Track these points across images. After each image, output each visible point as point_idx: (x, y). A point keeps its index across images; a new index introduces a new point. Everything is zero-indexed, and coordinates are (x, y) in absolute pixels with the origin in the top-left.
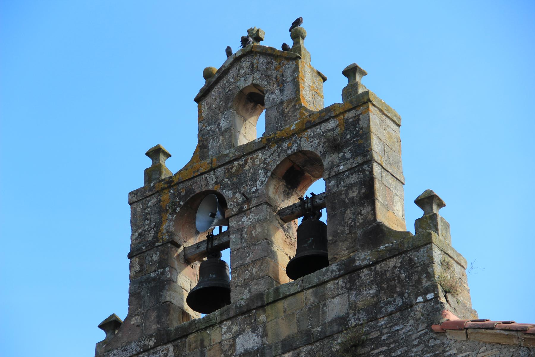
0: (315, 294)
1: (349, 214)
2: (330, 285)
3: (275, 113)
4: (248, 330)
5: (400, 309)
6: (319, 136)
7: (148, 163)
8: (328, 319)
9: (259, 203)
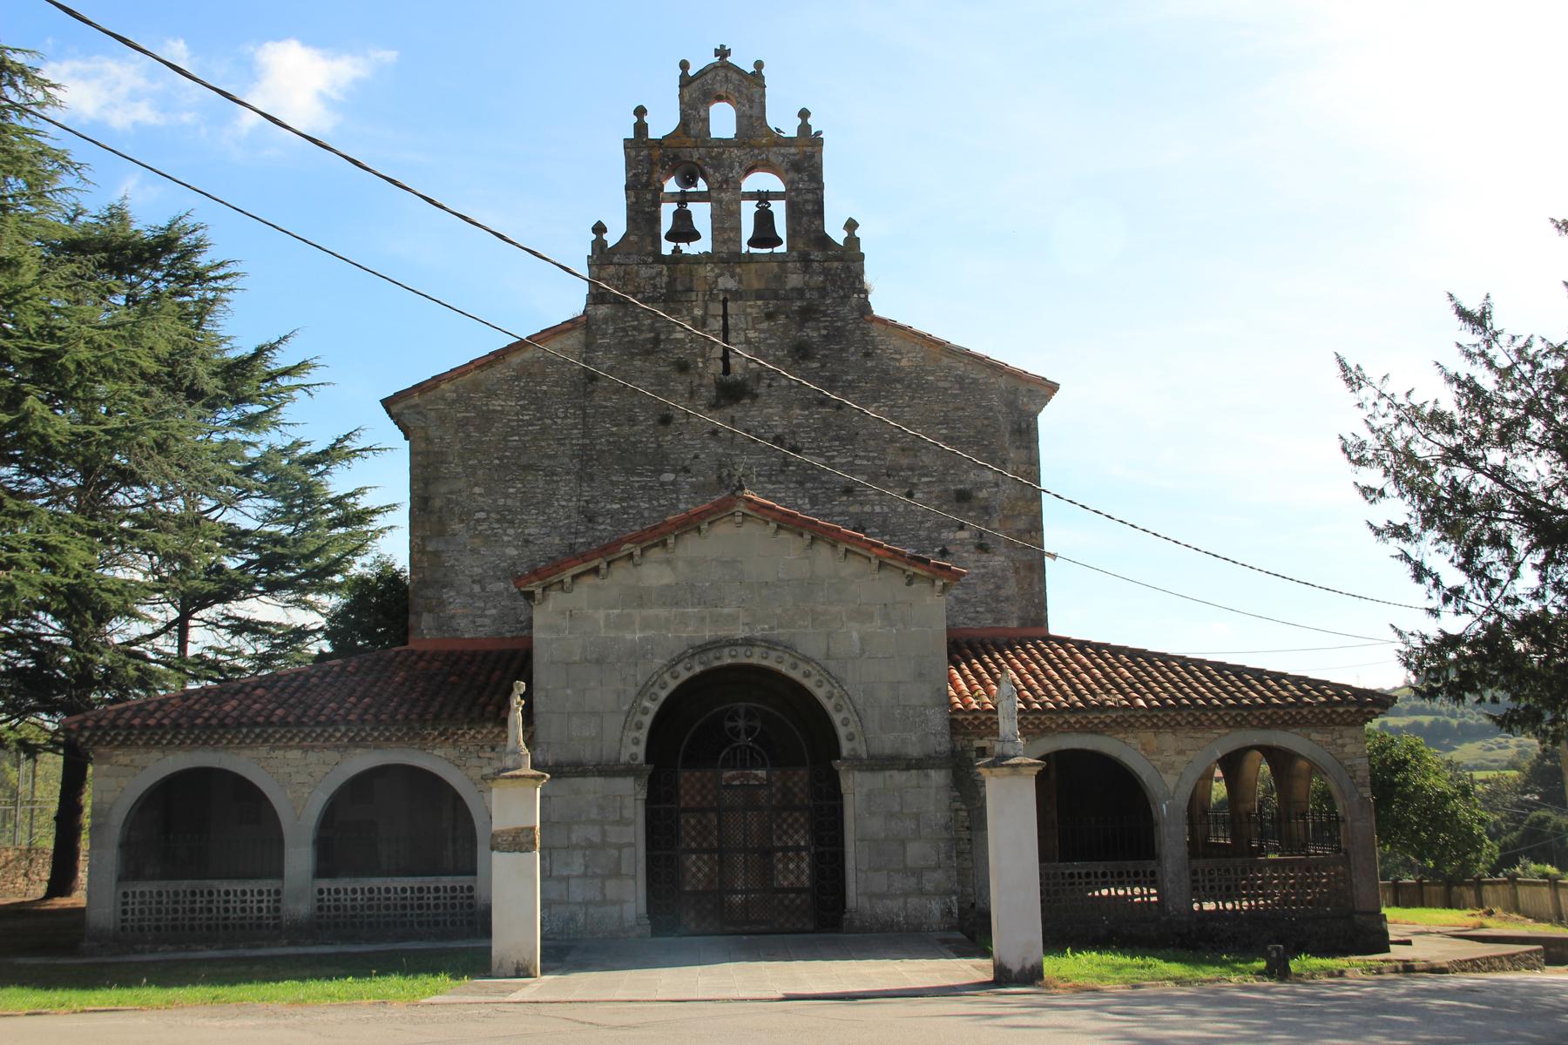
0: (779, 266)
1: (805, 219)
2: (789, 264)
3: (746, 123)
4: (727, 274)
5: (842, 297)
6: (784, 156)
7: (635, 119)
8: (517, 414)
9: (990, 1022)
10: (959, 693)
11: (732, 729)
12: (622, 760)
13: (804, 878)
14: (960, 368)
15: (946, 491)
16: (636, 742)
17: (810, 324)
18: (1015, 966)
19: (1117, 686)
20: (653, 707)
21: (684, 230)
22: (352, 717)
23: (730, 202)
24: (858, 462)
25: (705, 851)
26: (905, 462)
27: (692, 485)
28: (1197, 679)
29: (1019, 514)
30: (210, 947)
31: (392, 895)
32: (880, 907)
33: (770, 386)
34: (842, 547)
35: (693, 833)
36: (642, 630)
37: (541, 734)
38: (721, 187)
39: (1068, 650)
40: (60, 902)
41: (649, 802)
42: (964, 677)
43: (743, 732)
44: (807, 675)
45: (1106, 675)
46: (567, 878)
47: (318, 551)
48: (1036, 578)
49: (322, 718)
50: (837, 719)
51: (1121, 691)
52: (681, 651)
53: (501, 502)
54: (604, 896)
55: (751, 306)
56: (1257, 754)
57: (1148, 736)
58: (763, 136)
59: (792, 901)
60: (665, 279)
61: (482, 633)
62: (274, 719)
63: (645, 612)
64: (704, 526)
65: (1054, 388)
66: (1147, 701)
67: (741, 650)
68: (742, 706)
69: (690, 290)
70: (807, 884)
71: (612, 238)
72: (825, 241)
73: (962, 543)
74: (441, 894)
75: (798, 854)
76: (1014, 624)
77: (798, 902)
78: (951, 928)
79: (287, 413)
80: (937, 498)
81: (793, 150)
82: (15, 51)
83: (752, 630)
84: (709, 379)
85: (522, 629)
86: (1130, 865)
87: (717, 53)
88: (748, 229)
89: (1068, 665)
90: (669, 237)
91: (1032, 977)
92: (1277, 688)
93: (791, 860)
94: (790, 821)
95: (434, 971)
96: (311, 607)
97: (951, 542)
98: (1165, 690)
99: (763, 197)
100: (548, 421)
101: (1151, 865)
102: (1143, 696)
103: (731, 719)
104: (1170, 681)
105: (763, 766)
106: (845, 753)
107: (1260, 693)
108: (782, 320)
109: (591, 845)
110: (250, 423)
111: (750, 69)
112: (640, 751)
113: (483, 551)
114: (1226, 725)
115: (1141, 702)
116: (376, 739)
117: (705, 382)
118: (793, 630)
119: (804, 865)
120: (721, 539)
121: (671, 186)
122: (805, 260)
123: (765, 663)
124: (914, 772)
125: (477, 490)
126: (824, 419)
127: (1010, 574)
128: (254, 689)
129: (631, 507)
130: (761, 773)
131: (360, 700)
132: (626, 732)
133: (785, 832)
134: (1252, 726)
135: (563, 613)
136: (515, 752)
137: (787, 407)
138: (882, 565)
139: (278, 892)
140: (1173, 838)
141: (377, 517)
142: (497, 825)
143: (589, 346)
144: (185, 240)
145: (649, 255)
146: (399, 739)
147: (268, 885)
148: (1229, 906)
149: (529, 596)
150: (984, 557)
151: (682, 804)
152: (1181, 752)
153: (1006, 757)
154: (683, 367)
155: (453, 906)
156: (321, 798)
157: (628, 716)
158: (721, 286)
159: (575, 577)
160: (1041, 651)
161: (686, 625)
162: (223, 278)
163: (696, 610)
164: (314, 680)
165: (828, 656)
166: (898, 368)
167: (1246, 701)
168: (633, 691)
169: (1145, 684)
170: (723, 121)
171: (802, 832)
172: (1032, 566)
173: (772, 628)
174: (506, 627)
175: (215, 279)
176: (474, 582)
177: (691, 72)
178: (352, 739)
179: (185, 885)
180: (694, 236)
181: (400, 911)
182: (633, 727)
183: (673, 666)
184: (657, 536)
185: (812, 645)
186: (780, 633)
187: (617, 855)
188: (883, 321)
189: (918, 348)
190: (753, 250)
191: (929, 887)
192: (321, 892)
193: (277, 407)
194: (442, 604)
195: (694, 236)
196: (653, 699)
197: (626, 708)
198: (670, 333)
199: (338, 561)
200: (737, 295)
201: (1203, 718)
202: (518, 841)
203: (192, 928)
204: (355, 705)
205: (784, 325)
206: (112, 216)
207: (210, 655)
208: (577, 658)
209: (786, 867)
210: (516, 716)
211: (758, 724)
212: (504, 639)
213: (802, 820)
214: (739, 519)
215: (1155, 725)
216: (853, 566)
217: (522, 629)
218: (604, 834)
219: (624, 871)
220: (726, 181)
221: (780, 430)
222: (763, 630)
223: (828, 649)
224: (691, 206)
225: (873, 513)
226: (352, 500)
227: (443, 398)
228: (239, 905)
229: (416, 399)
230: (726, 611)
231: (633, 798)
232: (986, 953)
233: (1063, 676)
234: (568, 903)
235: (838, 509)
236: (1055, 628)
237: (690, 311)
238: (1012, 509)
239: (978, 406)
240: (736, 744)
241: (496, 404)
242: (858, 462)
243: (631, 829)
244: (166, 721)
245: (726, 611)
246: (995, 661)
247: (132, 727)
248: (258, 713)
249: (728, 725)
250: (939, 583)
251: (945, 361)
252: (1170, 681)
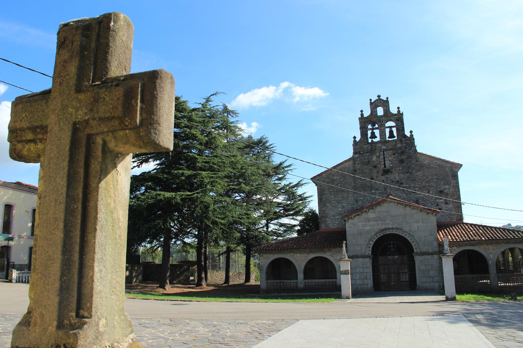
1: (400, 132)
5: (410, 148)
7: (361, 113)
10: (441, 238)
11: (390, 247)
12: (366, 254)
13: (407, 279)
14: (439, 163)
15: (437, 191)
16: (369, 251)
17: (403, 155)
18: (450, 297)
19: (478, 235)
20: (372, 243)
21: (373, 136)
22: (309, 247)
23: (383, 129)
24: (416, 185)
26: (427, 185)
27: (379, 193)
28: (498, 233)
29: (455, 195)
30: (284, 293)
31: (320, 283)
32: (424, 285)
33: (395, 170)
34: (412, 207)
35: (382, 270)
36: (369, 227)
37: (349, 249)
38: (381, 126)
39: (468, 226)
40: (248, 284)
41: (372, 263)
42: (442, 234)
44: (406, 235)
45: (476, 232)
46: (356, 279)
47: (297, 207)
48: (460, 209)
49: (304, 247)
50: (413, 244)
51: (479, 236)
53: (337, 199)
54: (364, 283)
55: (390, 152)
56: (518, 249)
57: (486, 246)
58: (389, 114)
60: (370, 148)
61: (335, 227)
62: (294, 248)
64: (381, 204)
65: (461, 165)
66: (485, 238)
67: (391, 230)
68: (391, 242)
69: (376, 150)
70: (408, 280)
71: (358, 139)
72: (405, 136)
73: (442, 202)
74: (330, 283)
76: (455, 220)
78: (441, 290)
79: (288, 176)
80: (435, 192)
81: (396, 117)
84: (381, 169)
85: (344, 226)
86: (483, 275)
87: (378, 96)
88: (388, 135)
89: (467, 230)
90: (370, 138)
91: (454, 299)
92: (517, 234)
95: (331, 298)
96: (296, 220)
97: (439, 202)
98: (490, 235)
99: (390, 127)
100: (346, 181)
101: (488, 275)
102: (484, 237)
104: (491, 233)
105: (397, 255)
106: (415, 252)
107: (513, 236)
108: (397, 155)
109: (360, 272)
110: (280, 179)
111: (385, 99)
112: (370, 252)
113: (334, 209)
114: (504, 243)
115: (483, 239)
116: (315, 251)
117: (380, 170)
119: (407, 276)
120: (385, 207)
121: (370, 127)
122: (401, 141)
123: (396, 233)
124: (431, 255)
125: (332, 196)
126: (408, 176)
127: (453, 209)
128: (289, 241)
129: (365, 198)
130: (397, 257)
131: (311, 243)
134: (511, 243)
135: (352, 224)
136: (344, 255)
137: (399, 174)
138: (421, 211)
139: (297, 282)
140: (493, 270)
141: (308, 198)
142: (342, 269)
143: (354, 164)
144: (264, 141)
145: (366, 143)
146: (319, 251)
147: (295, 281)
148: (508, 284)
149: (345, 221)
150: (447, 205)
151: (380, 263)
152: (493, 250)
153: (446, 254)
154: (375, 167)
155: (332, 285)
156: (304, 264)
158: (382, 148)
159: (354, 216)
160: (461, 226)
161: (379, 225)
162: (272, 148)
164: (301, 239)
165: (410, 231)
166: (424, 164)
167: (509, 238)
168: (368, 240)
169: (485, 234)
170: (380, 111)
172: (458, 206)
173: (397, 225)
174: (340, 226)
175: (270, 148)
176: (332, 216)
177: (372, 101)
178: (310, 251)
179: (278, 281)
180: (376, 137)
181: (321, 286)
184: (372, 207)
185: (406, 228)
186: (399, 226)
188: (420, 153)
189: (428, 159)
190: (390, 139)
191: (435, 281)
192: (305, 282)
193: (285, 175)
194: (326, 221)
195: (376, 137)
196: (372, 241)
197: (366, 243)
198: (372, 159)
199: (301, 210)
200: (386, 150)
201: (499, 242)
202: (346, 273)
203: (280, 289)
204: (310, 244)
205: (397, 156)
206: (249, 137)
207: (274, 230)
208: (356, 233)
209: (403, 277)
210: (344, 248)
211: (395, 246)
212: (339, 228)
214: (389, 202)
215: (487, 244)
216: (415, 211)
217: (344, 226)
218: (363, 270)
219: (368, 278)
220: (382, 125)
221: (398, 179)
224: (374, 131)
225: (420, 197)
226: (303, 195)
227: (324, 177)
228: (289, 285)
229: (318, 178)
230: (387, 222)
232: (444, 295)
233: (466, 233)
234: (356, 285)
235: (412, 196)
236: (465, 221)
237: (376, 154)
238: (453, 194)
239: (444, 171)
241: (335, 178)
242: (416, 185)
244: (273, 248)
245: (387, 222)
246: (450, 229)
247: (267, 250)
248: (291, 246)
249: (389, 246)
250: (434, 214)
251: (435, 161)
252: (491, 233)
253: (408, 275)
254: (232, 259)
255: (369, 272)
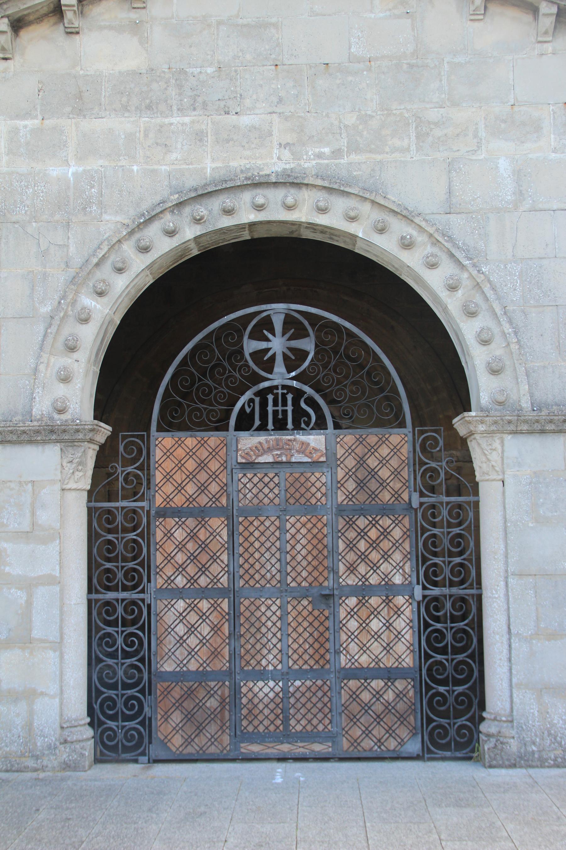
11: (258, 355)
13: (400, 648)
25: (204, 593)
43: (279, 359)
52: (158, 199)
59: (378, 695)
63: (86, 125)
70: (408, 661)
75: (388, 601)
77: (390, 696)
82: (217, 700)
83: (296, 156)
93: (375, 613)
94: (373, 534)
103: (257, 335)
118: (379, 157)
119: (400, 624)
123: (322, 220)
132: (45, 356)
133: (363, 557)
151: (159, 501)
157: (50, 325)
163: (187, 120)
171: (397, 556)
173: (337, 153)
182: (60, 345)
183: (141, 227)
187: (23, 601)
197: (46, 309)
209: (364, 625)
213: (397, 533)
219: (36, 634)
222: (320, 156)
223: (450, 192)
230: (246, 120)
231: (58, 487)
240: (266, 384)
243: (53, 548)
245: (246, 120)
253: (408, 612)
254: (289, 192)
255: (50, 580)
